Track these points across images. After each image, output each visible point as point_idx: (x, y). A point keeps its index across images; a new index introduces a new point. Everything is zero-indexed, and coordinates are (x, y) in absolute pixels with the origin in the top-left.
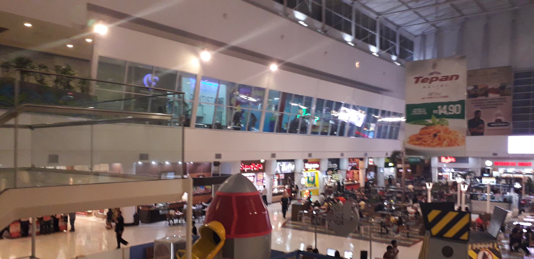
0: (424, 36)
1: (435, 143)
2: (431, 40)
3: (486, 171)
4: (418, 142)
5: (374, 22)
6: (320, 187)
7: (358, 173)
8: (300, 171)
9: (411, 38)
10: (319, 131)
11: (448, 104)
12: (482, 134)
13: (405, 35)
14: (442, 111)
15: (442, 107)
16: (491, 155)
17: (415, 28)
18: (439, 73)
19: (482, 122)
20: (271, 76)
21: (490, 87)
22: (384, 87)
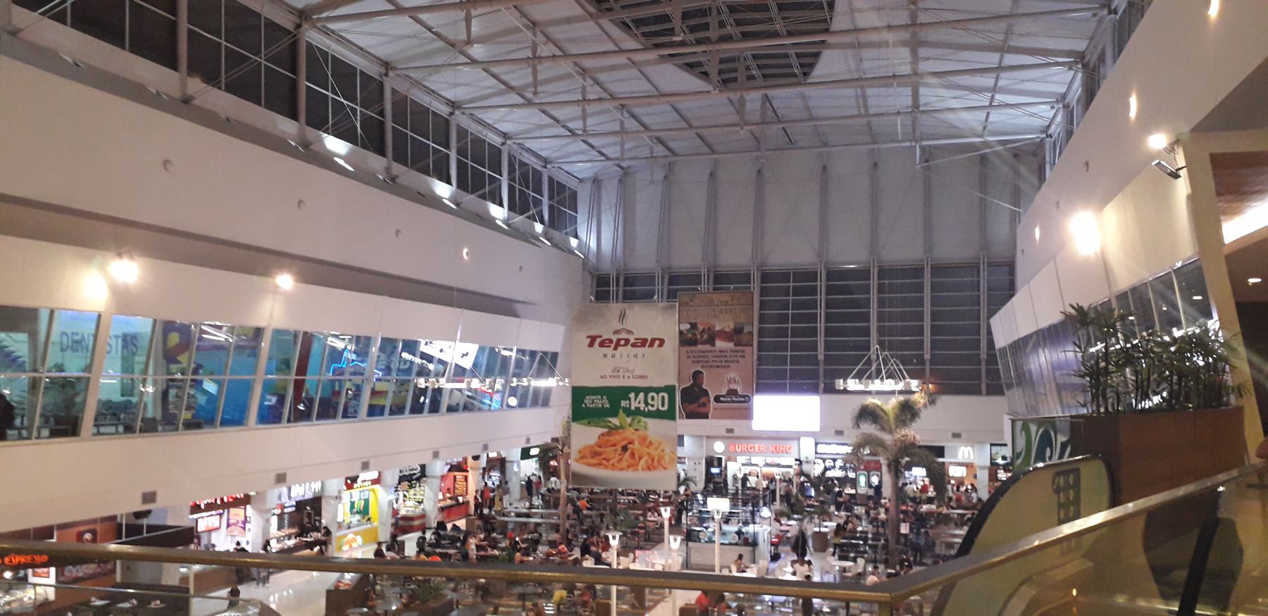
0: (596, 182)
1: (624, 464)
2: (610, 195)
3: (716, 463)
4: (594, 461)
5: (496, 152)
6: (381, 523)
7: (466, 478)
8: (336, 494)
9: (572, 184)
10: (387, 402)
11: (647, 390)
12: (705, 416)
13: (562, 178)
14: (636, 402)
15: (636, 397)
16: (723, 433)
17: (577, 165)
18: (630, 332)
19: (706, 393)
20: (278, 302)
21: (717, 328)
22: (520, 299)
